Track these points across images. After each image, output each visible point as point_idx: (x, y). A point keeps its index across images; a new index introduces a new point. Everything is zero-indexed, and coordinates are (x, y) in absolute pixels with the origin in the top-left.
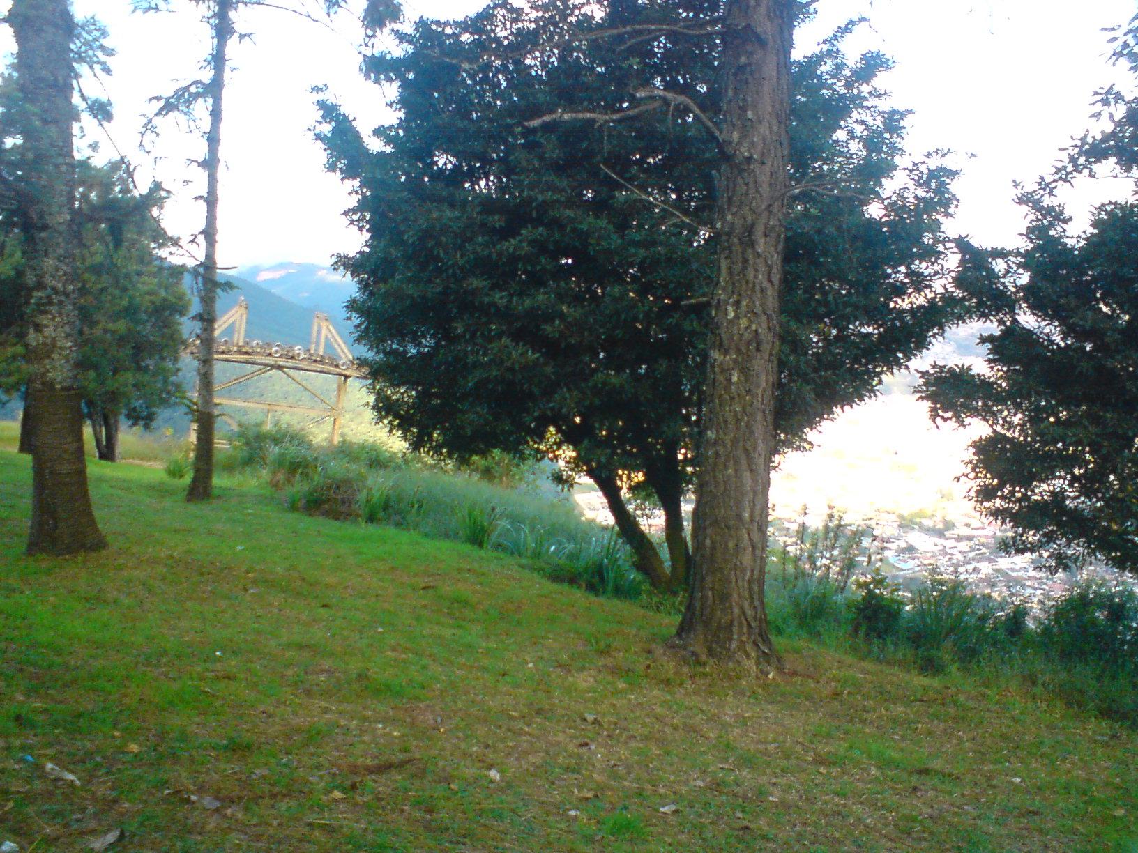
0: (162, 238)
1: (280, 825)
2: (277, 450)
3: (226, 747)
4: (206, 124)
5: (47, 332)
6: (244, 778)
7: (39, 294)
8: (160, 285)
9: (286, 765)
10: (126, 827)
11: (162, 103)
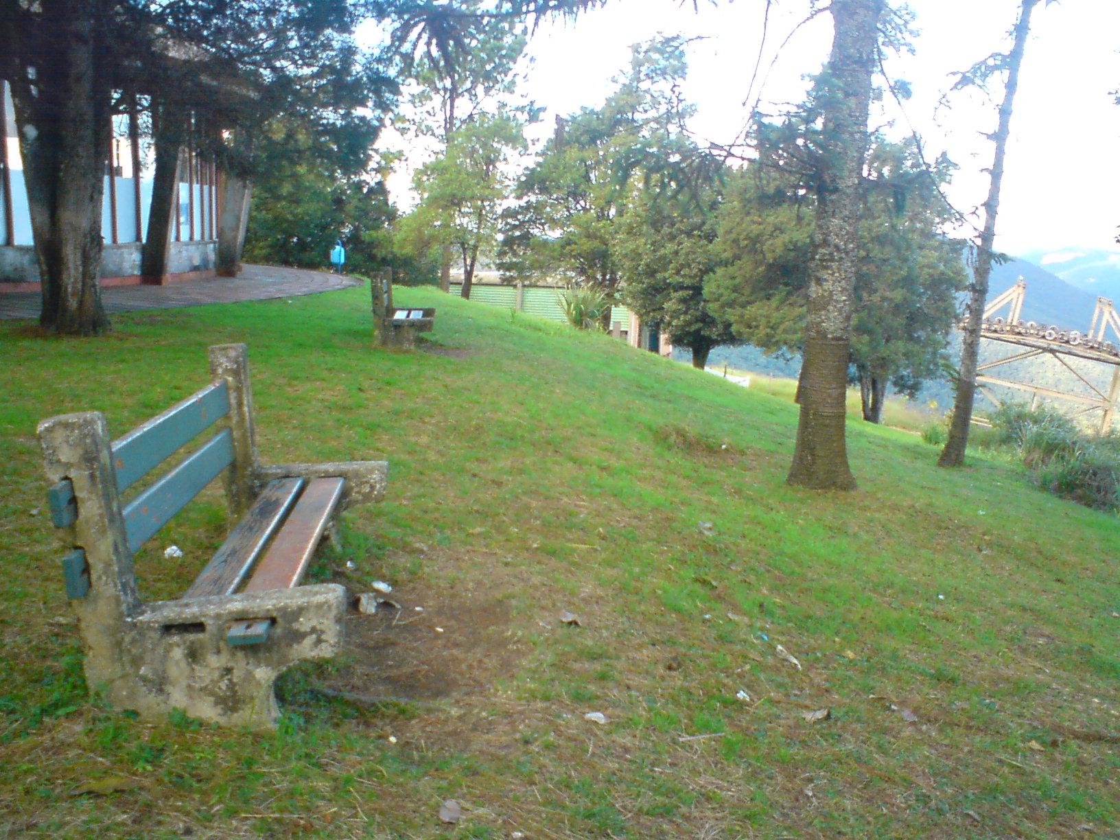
0: (946, 212)
1: (970, 752)
2: (1035, 429)
3: (932, 676)
4: (999, 95)
5: (827, 285)
6: (944, 705)
7: (824, 251)
8: (940, 259)
9: (988, 706)
10: (833, 712)
11: (959, 77)
